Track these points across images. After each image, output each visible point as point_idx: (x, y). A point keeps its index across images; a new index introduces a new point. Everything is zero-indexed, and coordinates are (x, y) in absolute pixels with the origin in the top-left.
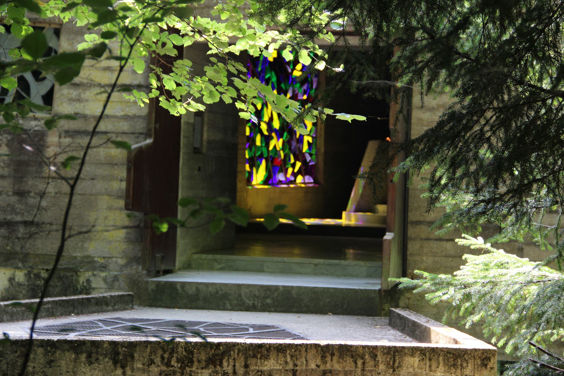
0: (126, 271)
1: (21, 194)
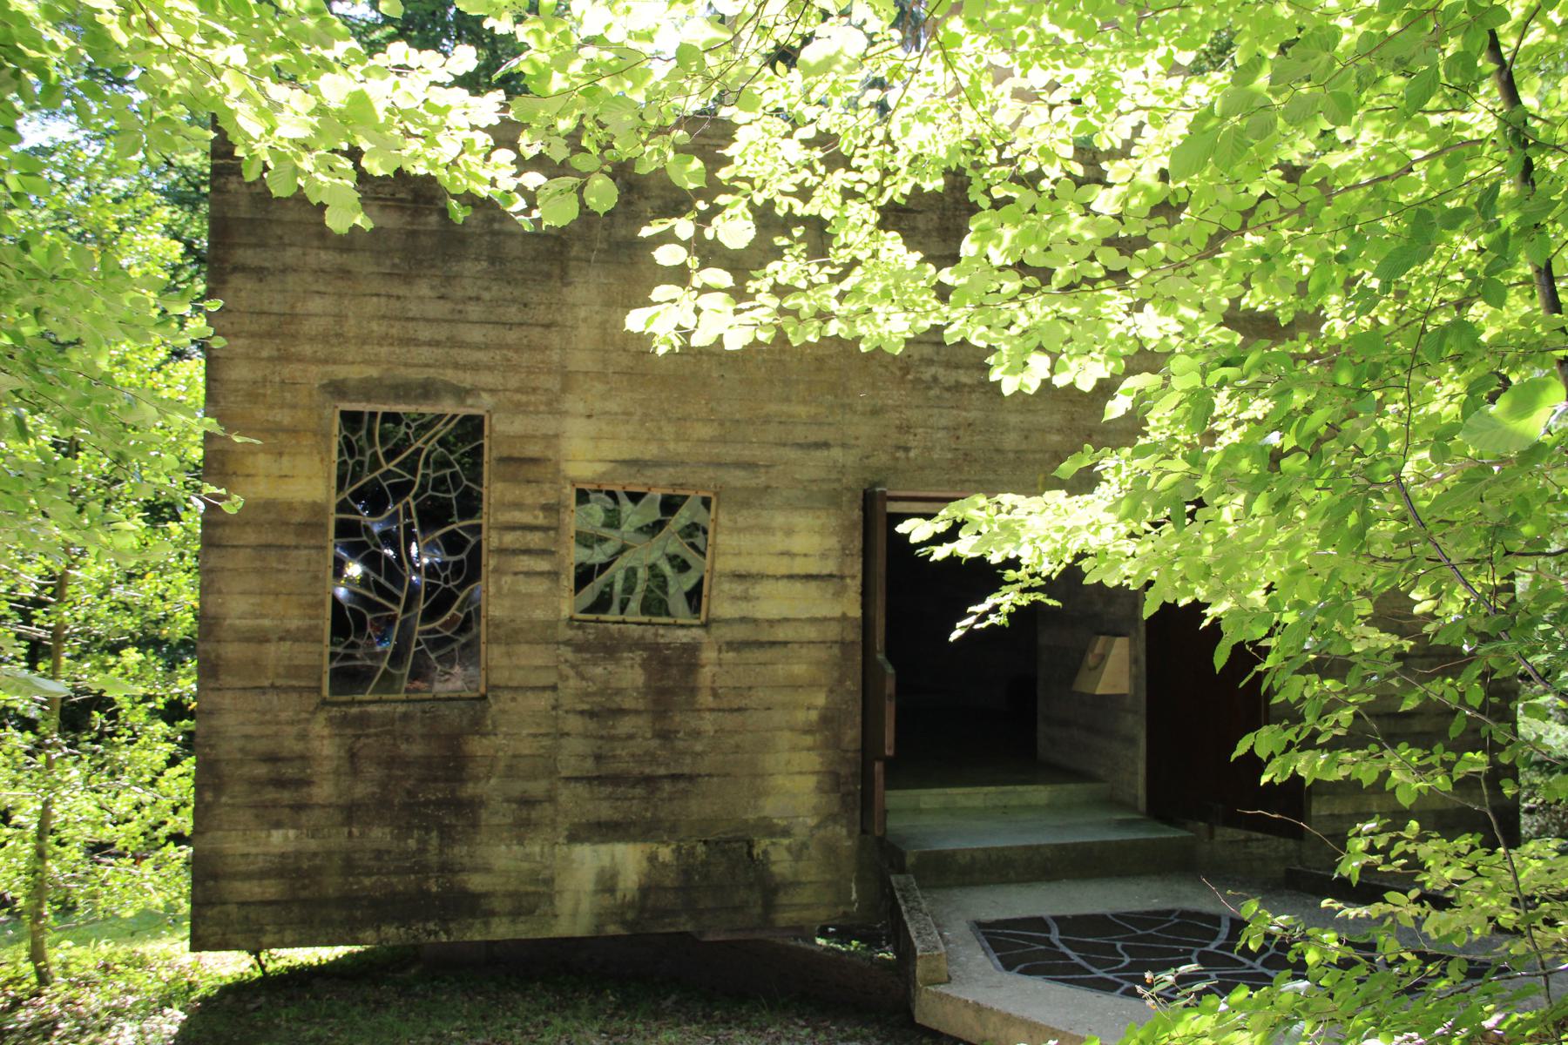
0: (821, 833)
1: (665, 736)
